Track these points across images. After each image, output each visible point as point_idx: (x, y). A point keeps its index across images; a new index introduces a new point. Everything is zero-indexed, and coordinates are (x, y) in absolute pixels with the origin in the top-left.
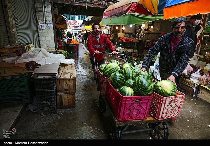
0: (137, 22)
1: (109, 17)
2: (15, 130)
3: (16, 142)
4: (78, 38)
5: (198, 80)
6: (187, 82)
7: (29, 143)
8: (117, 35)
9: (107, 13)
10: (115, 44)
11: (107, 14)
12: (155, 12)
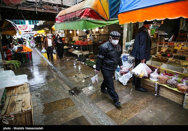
0: (92, 27)
1: (62, 22)
2: (13, 117)
3: (14, 127)
4: (31, 43)
5: (157, 79)
6: (148, 82)
7: (26, 129)
8: (71, 38)
9: (59, 18)
10: (70, 47)
11: (60, 19)
12: (107, 17)
